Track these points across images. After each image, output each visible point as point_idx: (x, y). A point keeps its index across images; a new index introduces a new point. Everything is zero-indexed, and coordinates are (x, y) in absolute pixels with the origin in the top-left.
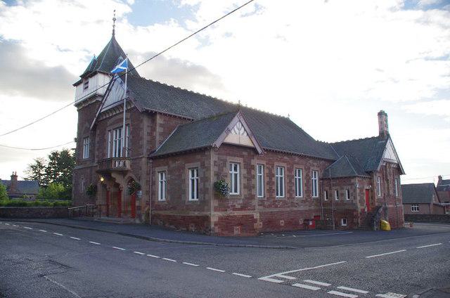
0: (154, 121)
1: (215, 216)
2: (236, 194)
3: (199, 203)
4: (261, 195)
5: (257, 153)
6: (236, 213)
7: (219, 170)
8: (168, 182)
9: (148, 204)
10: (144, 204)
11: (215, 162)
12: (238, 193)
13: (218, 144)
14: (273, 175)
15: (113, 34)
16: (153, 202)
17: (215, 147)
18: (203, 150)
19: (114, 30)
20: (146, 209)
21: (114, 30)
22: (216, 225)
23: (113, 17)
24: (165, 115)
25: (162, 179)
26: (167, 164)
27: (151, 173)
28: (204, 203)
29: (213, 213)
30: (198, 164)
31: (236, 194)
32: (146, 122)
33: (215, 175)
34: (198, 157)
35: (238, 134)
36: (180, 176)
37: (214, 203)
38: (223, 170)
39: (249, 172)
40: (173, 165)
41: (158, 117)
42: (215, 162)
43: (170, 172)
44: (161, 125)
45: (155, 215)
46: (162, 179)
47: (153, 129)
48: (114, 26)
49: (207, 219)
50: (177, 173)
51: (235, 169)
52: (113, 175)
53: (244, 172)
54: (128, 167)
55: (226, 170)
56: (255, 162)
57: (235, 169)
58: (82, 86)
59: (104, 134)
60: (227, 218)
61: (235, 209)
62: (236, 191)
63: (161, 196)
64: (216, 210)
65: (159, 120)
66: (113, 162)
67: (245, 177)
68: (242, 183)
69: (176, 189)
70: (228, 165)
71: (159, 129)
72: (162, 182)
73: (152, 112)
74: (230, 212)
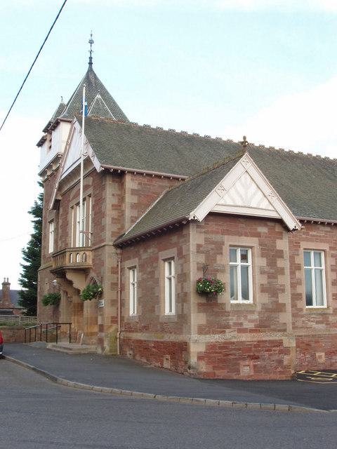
0: (122, 185)
1: (197, 345)
2: (246, 302)
3: (176, 320)
4: (323, 305)
5: (286, 228)
6: (245, 338)
7: (207, 258)
8: (140, 283)
9: (114, 320)
10: (107, 322)
11: (199, 246)
12: (250, 301)
13: (200, 213)
14: (299, 268)
15: (91, 63)
16: (122, 318)
17: (195, 221)
18: (180, 227)
19: (91, 58)
20: (112, 330)
21: (91, 58)
22: (200, 358)
23: (89, 38)
24: (139, 174)
25: (170, 274)
26: (137, 255)
27: (118, 271)
28: (182, 318)
29: (194, 336)
30: (173, 252)
31: (246, 302)
32: (110, 189)
33: (198, 269)
34: (174, 239)
35: (244, 191)
36: (152, 273)
37: (197, 319)
38: (215, 260)
39: (272, 263)
40: (145, 256)
41: (128, 178)
42: (199, 246)
43: (142, 267)
44: (134, 192)
45: (124, 340)
46: (170, 274)
47: (122, 199)
48: (91, 52)
49: (183, 348)
50: (149, 270)
51: (244, 258)
52: (69, 276)
53: (263, 262)
54: (90, 262)
55: (223, 260)
56: (283, 244)
57: (244, 258)
58: (47, 144)
59: (67, 214)
60: (225, 346)
61: (242, 331)
62: (245, 296)
63: (133, 309)
64: (201, 331)
65: (130, 183)
66: (68, 254)
67: (262, 272)
68: (257, 282)
69: (150, 297)
70: (226, 249)
71: (130, 199)
72: (170, 279)
73: (115, 171)
74: (231, 335)
